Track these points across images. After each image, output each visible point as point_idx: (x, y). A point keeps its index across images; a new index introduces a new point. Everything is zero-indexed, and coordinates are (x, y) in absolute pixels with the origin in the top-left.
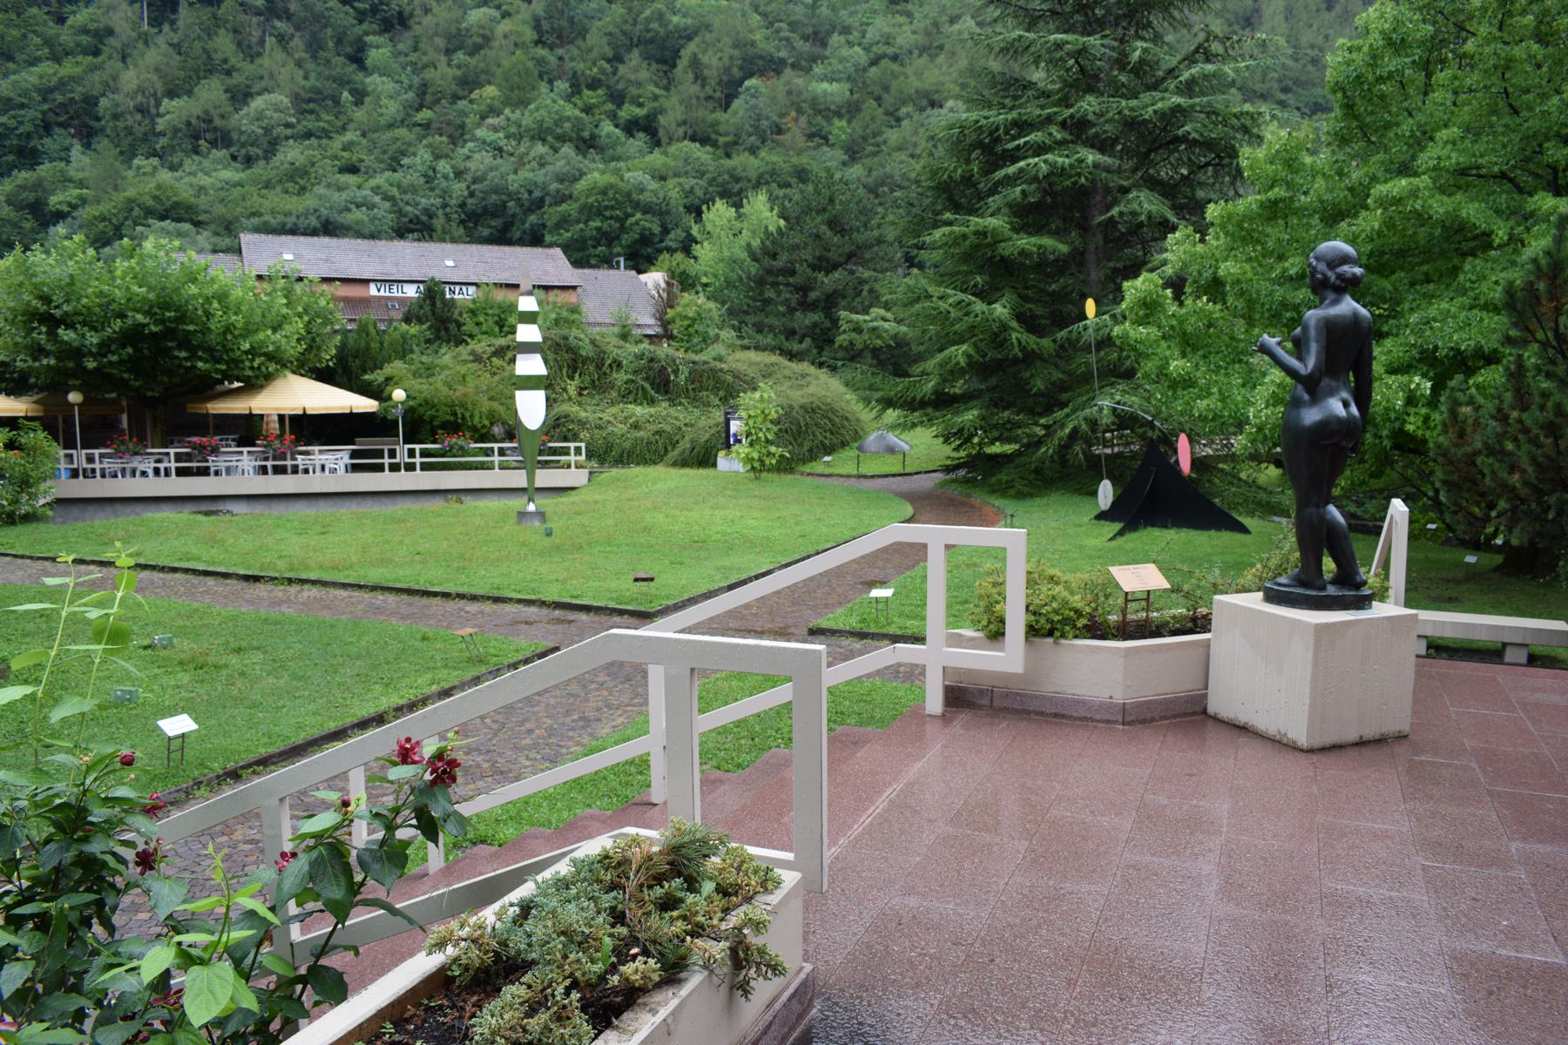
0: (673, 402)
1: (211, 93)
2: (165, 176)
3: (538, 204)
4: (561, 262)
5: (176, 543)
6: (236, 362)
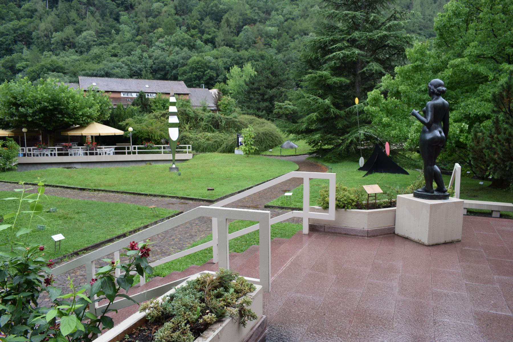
0: (220, 132)
1: (69, 30)
2: (54, 58)
3: (176, 67)
4: (184, 86)
5: (58, 178)
6: (77, 119)
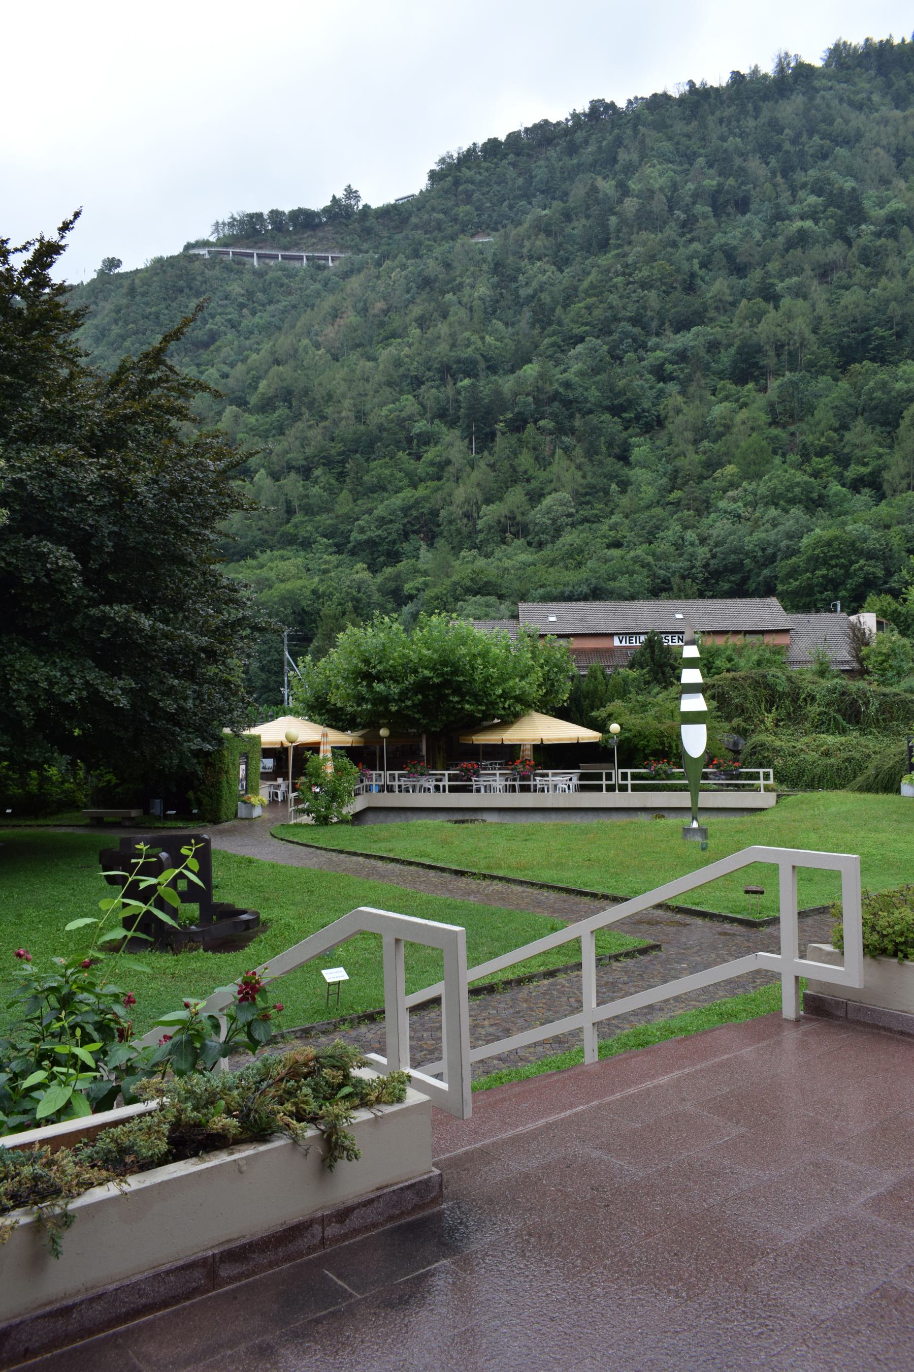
0: (863, 732)
1: (516, 497)
2: (481, 562)
3: (772, 559)
4: (776, 609)
5: (420, 843)
6: (493, 704)
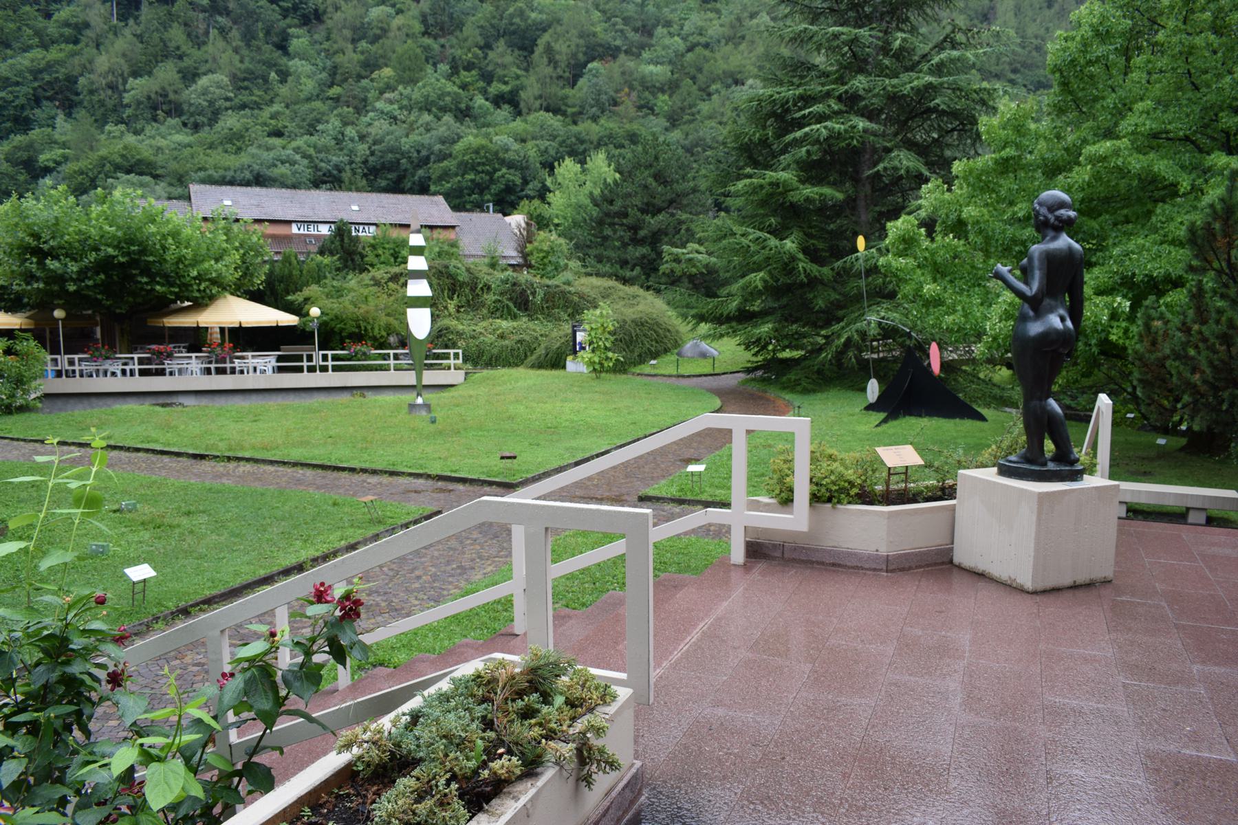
0: (531, 318)
1: (167, 73)
2: (130, 139)
3: (425, 161)
4: (443, 207)
5: (139, 429)
6: (186, 286)
